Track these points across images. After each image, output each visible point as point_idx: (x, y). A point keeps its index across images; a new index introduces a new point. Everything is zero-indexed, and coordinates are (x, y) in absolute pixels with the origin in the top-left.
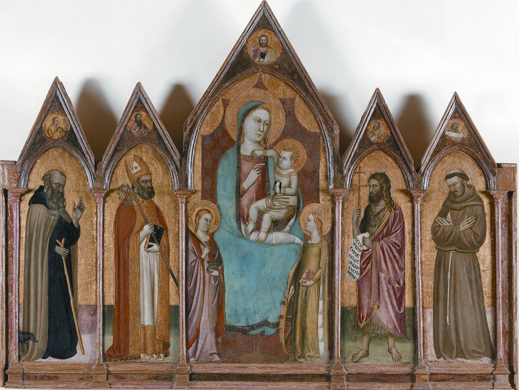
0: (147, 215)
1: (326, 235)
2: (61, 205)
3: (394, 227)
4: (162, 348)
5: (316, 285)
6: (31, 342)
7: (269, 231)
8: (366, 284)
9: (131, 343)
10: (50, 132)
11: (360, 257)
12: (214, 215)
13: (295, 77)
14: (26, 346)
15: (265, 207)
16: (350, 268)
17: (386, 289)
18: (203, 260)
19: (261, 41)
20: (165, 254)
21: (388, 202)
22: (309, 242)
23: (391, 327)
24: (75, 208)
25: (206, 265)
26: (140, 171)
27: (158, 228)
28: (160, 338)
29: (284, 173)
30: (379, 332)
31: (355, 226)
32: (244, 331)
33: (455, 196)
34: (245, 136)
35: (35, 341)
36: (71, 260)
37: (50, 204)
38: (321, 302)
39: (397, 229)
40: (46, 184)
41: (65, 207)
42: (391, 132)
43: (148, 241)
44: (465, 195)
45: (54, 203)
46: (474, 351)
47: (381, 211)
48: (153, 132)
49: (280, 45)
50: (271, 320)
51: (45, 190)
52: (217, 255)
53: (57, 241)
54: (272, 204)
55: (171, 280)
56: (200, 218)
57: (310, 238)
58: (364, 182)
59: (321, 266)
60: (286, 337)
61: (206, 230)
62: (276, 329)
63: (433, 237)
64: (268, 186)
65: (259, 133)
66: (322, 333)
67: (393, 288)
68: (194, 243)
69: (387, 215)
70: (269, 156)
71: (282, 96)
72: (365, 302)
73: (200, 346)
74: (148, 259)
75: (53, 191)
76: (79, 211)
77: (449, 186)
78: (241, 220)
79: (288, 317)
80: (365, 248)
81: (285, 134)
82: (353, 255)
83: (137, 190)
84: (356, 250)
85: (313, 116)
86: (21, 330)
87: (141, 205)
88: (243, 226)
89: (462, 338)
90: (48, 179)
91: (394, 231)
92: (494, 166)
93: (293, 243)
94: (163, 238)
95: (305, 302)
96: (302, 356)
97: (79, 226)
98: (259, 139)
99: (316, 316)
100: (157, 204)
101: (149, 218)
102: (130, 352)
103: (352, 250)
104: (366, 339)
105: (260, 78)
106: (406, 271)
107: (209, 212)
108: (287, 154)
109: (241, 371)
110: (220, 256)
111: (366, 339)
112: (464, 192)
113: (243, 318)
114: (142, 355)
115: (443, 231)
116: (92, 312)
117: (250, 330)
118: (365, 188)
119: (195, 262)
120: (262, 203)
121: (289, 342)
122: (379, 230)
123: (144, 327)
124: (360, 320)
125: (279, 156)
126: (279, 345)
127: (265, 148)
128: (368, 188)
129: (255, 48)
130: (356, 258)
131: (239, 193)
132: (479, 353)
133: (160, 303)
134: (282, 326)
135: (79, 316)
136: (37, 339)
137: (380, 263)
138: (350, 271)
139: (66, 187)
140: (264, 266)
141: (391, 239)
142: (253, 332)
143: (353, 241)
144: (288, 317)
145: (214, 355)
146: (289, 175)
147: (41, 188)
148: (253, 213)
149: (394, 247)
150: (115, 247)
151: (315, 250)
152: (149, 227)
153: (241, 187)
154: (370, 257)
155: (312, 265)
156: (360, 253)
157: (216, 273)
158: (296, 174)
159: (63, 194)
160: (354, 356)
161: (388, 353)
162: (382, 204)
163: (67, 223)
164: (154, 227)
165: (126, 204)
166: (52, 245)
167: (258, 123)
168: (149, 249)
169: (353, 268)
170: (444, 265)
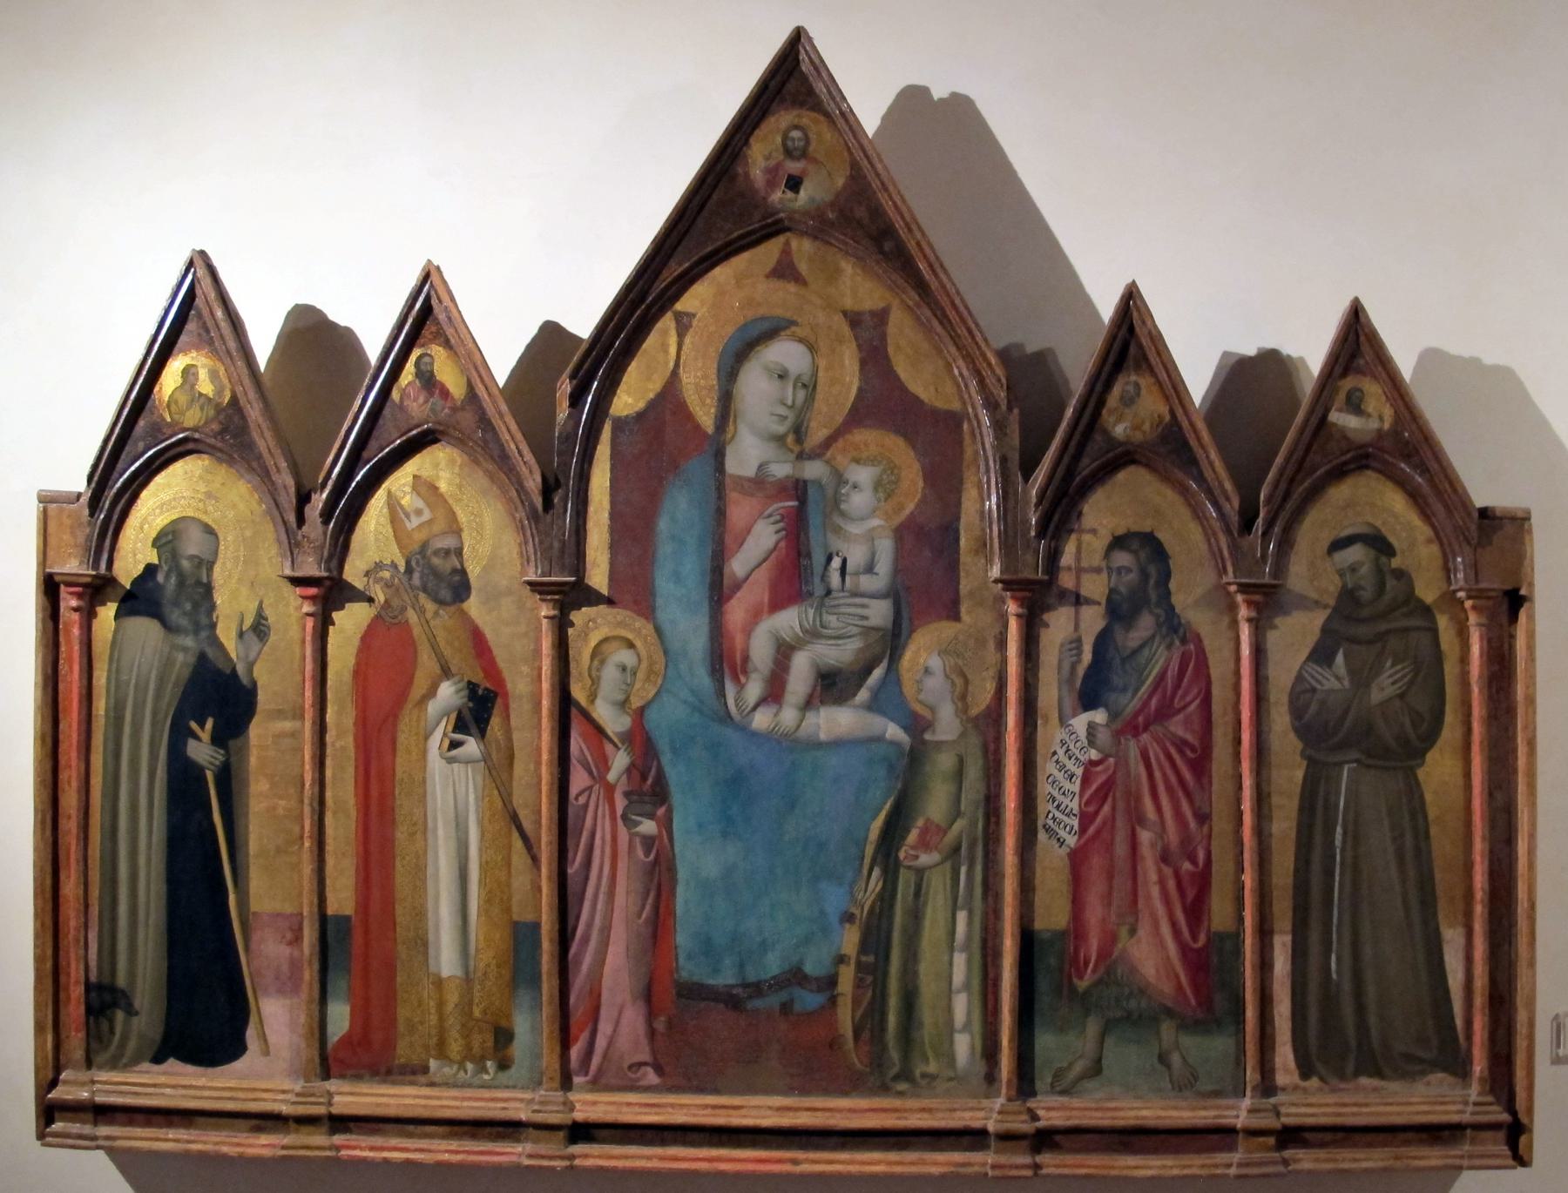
0: (447, 652)
1: (977, 718)
2: (204, 620)
3: (1180, 692)
4: (490, 1044)
5: (948, 865)
6: (120, 1015)
7: (808, 705)
8: (1096, 862)
9: (401, 1027)
10: (173, 407)
11: (1078, 782)
12: (643, 653)
13: (888, 246)
14: (105, 1026)
15: (798, 629)
16: (1051, 816)
17: (1154, 877)
18: (610, 789)
19: (790, 143)
20: (499, 769)
21: (1162, 619)
22: (928, 736)
23: (1167, 988)
24: (244, 629)
25: (620, 803)
26: (430, 522)
27: (480, 692)
28: (486, 1014)
29: (854, 529)
30: (1133, 1004)
31: (1065, 693)
32: (731, 1000)
33: (1357, 603)
34: (739, 421)
35: (131, 1012)
36: (228, 778)
37: (175, 616)
38: (962, 917)
39: (1188, 699)
40: (164, 557)
41: (213, 626)
42: (1172, 412)
43: (450, 728)
44: (1387, 597)
45: (185, 614)
46: (1409, 1058)
47: (1142, 647)
48: (467, 407)
49: (846, 154)
50: (809, 968)
51: (160, 578)
52: (653, 771)
53: (193, 725)
54: (818, 623)
55: (518, 844)
56: (602, 662)
57: (928, 725)
58: (1097, 560)
59: (963, 808)
60: (857, 1018)
61: (621, 697)
62: (828, 994)
63: (1297, 724)
64: (805, 570)
65: (782, 411)
66: (962, 1007)
67: (1177, 874)
68: (584, 736)
69: (1161, 659)
70: (812, 478)
71: (849, 303)
72: (1094, 914)
73: (601, 1043)
74: (451, 783)
75: (181, 583)
76: (255, 638)
77: (1341, 573)
78: (726, 670)
79: (864, 959)
80: (1094, 755)
81: (858, 416)
82: (1059, 776)
83: (421, 578)
84: (1066, 761)
85: (941, 363)
86: (93, 978)
87: (432, 623)
88: (730, 690)
89: (1372, 1020)
90: (170, 546)
91: (1182, 704)
92: (1469, 514)
93: (879, 739)
94: (495, 722)
95: (916, 915)
96: (905, 1075)
97: (255, 684)
98: (781, 429)
99: (946, 958)
100: (479, 621)
101: (455, 664)
102: (399, 1051)
103: (1057, 762)
104: (1093, 1027)
105: (786, 251)
106: (1213, 823)
107: (631, 645)
108: (863, 475)
109: (720, 1120)
110: (661, 779)
111: (1093, 1027)
112: (1381, 588)
113: (727, 962)
114: (433, 1064)
115: (1323, 703)
116: (289, 935)
117: (750, 997)
118: (1095, 576)
119: (586, 794)
120: (789, 620)
121: (866, 1035)
122: (1135, 704)
123: (439, 983)
124: (1078, 969)
125: (840, 479)
126: (834, 1043)
127: (801, 456)
128: (1105, 575)
129: (772, 163)
130: (1067, 785)
131: (719, 590)
132: (1421, 1061)
133: (484, 910)
134: (846, 983)
135: (253, 946)
136: (137, 1004)
137: (1138, 799)
138: (1050, 822)
139: (217, 569)
140: (793, 807)
141: (1172, 729)
142: (758, 1003)
143: (1060, 734)
144: (864, 959)
145: (643, 1069)
146: (870, 537)
147: (150, 570)
148: (761, 651)
149: (1181, 752)
150: (357, 747)
151: (945, 762)
152: (452, 689)
153: (726, 571)
154: (1108, 786)
155: (935, 805)
156: (1079, 772)
157: (648, 827)
158: (891, 534)
159: (208, 589)
160: (1058, 1075)
161: (1159, 1067)
162: (1146, 624)
163: (219, 672)
164: (468, 687)
165: (388, 619)
166: (180, 734)
167: (777, 383)
168: (454, 752)
169: (1058, 814)
170: (1326, 808)
